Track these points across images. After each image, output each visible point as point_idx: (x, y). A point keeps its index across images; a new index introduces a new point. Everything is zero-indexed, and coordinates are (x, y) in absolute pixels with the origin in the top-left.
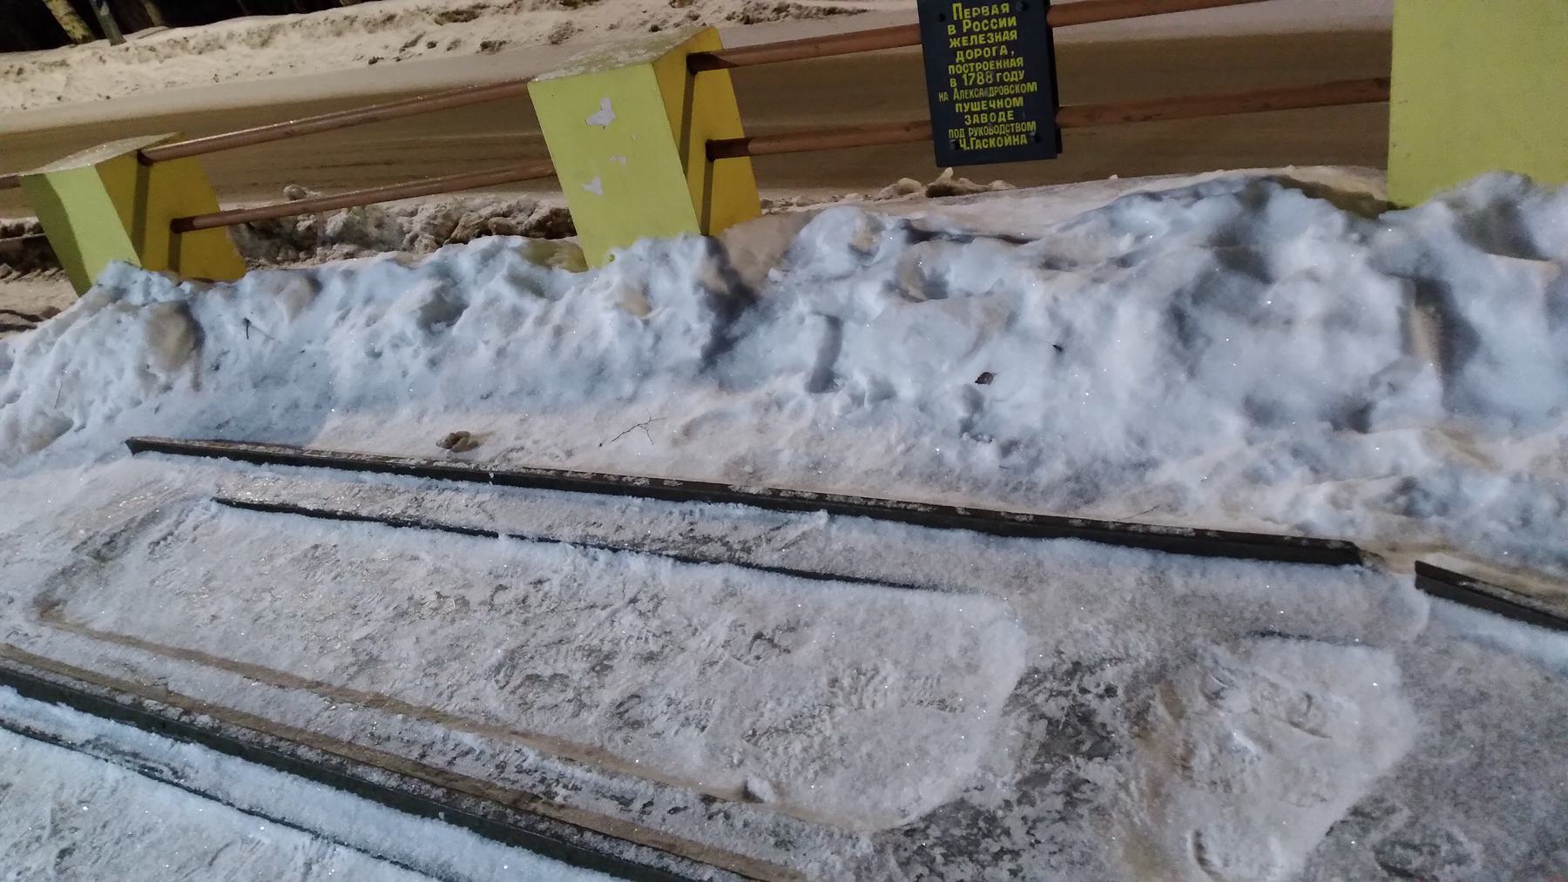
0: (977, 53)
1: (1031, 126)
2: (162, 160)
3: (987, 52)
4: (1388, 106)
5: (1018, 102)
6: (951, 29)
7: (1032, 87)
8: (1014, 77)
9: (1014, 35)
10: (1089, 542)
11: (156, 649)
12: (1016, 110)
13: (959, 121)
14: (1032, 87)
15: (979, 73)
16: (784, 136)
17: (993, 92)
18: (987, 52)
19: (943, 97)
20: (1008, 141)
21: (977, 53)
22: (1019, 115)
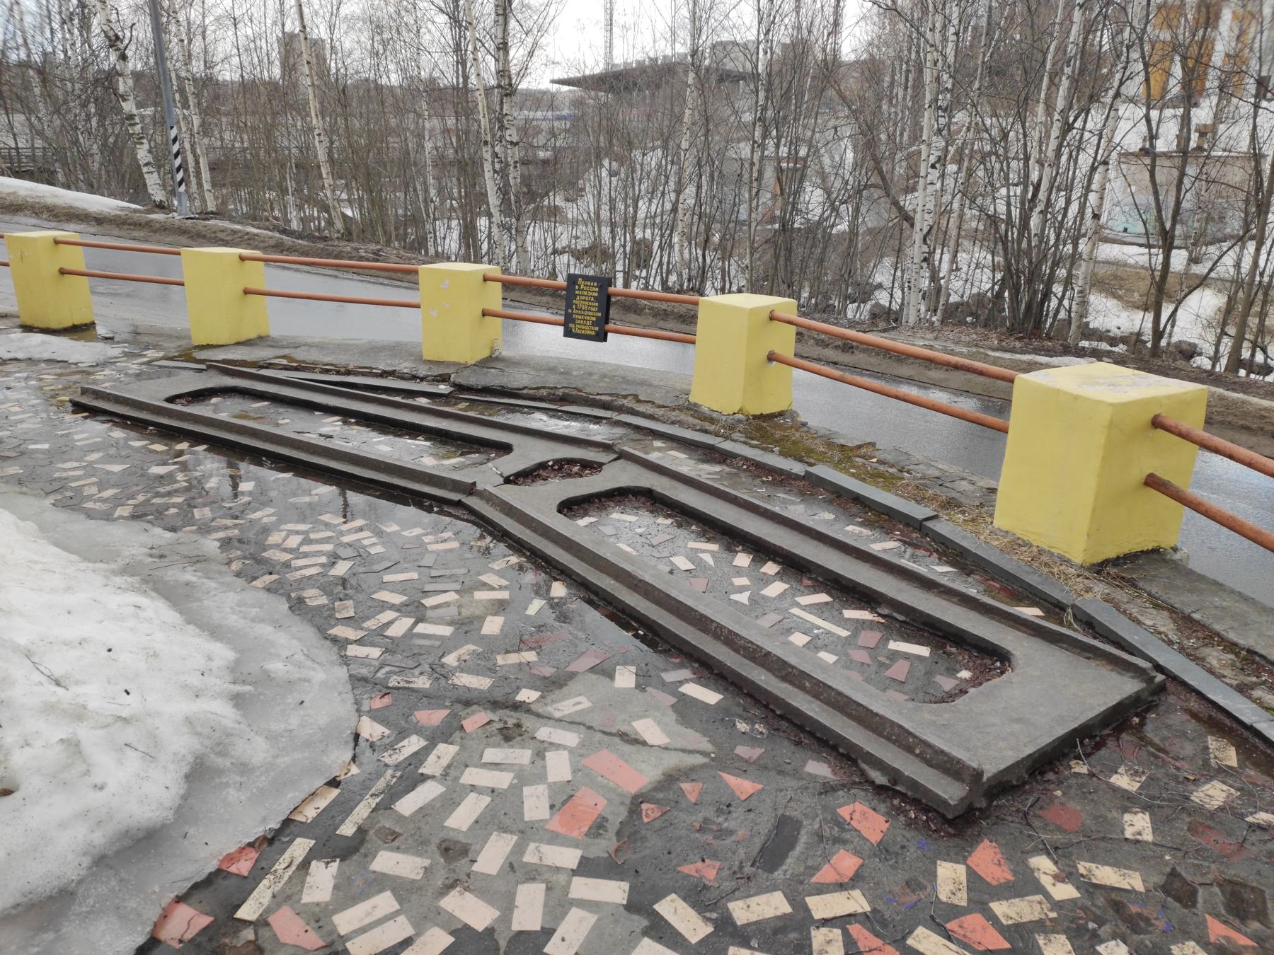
0: (583, 298)
1: (597, 329)
2: (779, 320)
3: (587, 298)
4: (1006, 438)
5: (594, 319)
6: (577, 287)
7: (599, 314)
8: (594, 309)
9: (596, 294)
10: (796, 533)
11: (531, 389)
12: (593, 322)
13: (573, 321)
14: (599, 314)
15: (584, 305)
16: (828, 363)
17: (587, 313)
18: (587, 298)
19: (570, 311)
20: (589, 332)
21: (583, 298)
22: (594, 324)
